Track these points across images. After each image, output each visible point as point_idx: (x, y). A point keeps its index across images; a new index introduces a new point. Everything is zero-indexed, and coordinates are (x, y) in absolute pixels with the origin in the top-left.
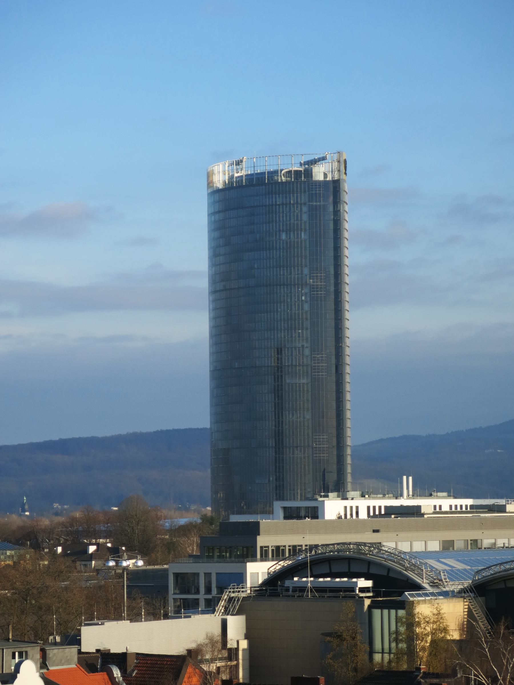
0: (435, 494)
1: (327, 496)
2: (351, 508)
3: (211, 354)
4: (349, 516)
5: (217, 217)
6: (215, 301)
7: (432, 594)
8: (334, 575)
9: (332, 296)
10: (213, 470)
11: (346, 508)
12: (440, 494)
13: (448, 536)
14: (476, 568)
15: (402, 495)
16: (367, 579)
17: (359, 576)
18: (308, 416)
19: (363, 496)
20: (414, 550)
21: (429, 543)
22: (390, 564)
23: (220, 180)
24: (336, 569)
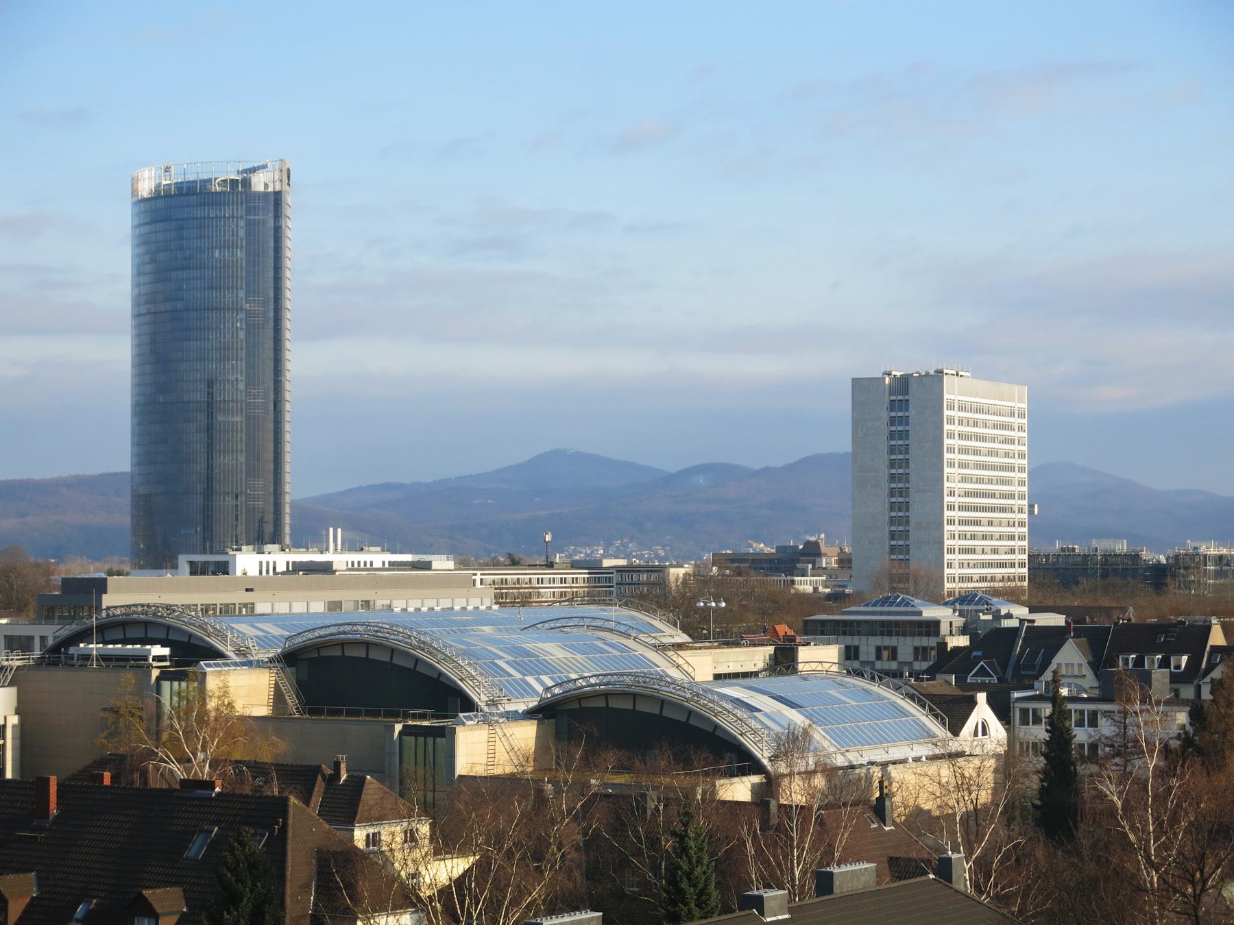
0: (366, 548)
1: (239, 550)
2: (268, 563)
3: (134, 386)
4: (264, 573)
5: (143, 230)
6: (138, 326)
7: (236, 664)
8: (125, 642)
9: (272, 323)
10: (133, 517)
11: (261, 563)
12: (372, 549)
13: (335, 596)
14: (287, 634)
15: (327, 549)
16: (163, 646)
17: (153, 642)
18: (242, 458)
19: (283, 550)
20: (312, 611)
21: (312, 604)
22: (191, 629)
23: (146, 188)
24: (131, 633)
